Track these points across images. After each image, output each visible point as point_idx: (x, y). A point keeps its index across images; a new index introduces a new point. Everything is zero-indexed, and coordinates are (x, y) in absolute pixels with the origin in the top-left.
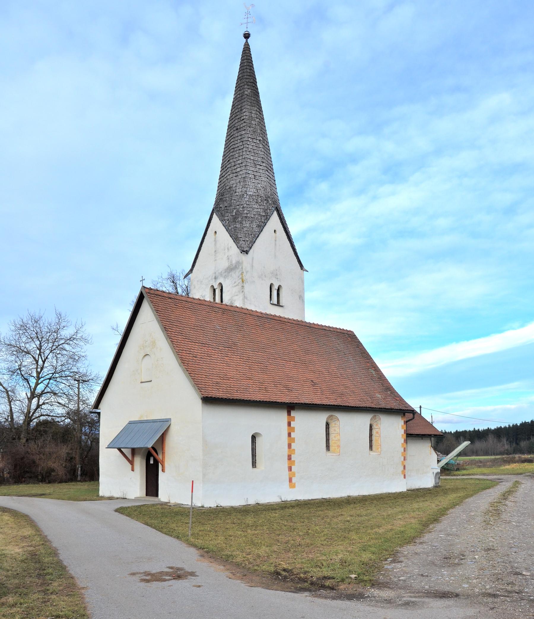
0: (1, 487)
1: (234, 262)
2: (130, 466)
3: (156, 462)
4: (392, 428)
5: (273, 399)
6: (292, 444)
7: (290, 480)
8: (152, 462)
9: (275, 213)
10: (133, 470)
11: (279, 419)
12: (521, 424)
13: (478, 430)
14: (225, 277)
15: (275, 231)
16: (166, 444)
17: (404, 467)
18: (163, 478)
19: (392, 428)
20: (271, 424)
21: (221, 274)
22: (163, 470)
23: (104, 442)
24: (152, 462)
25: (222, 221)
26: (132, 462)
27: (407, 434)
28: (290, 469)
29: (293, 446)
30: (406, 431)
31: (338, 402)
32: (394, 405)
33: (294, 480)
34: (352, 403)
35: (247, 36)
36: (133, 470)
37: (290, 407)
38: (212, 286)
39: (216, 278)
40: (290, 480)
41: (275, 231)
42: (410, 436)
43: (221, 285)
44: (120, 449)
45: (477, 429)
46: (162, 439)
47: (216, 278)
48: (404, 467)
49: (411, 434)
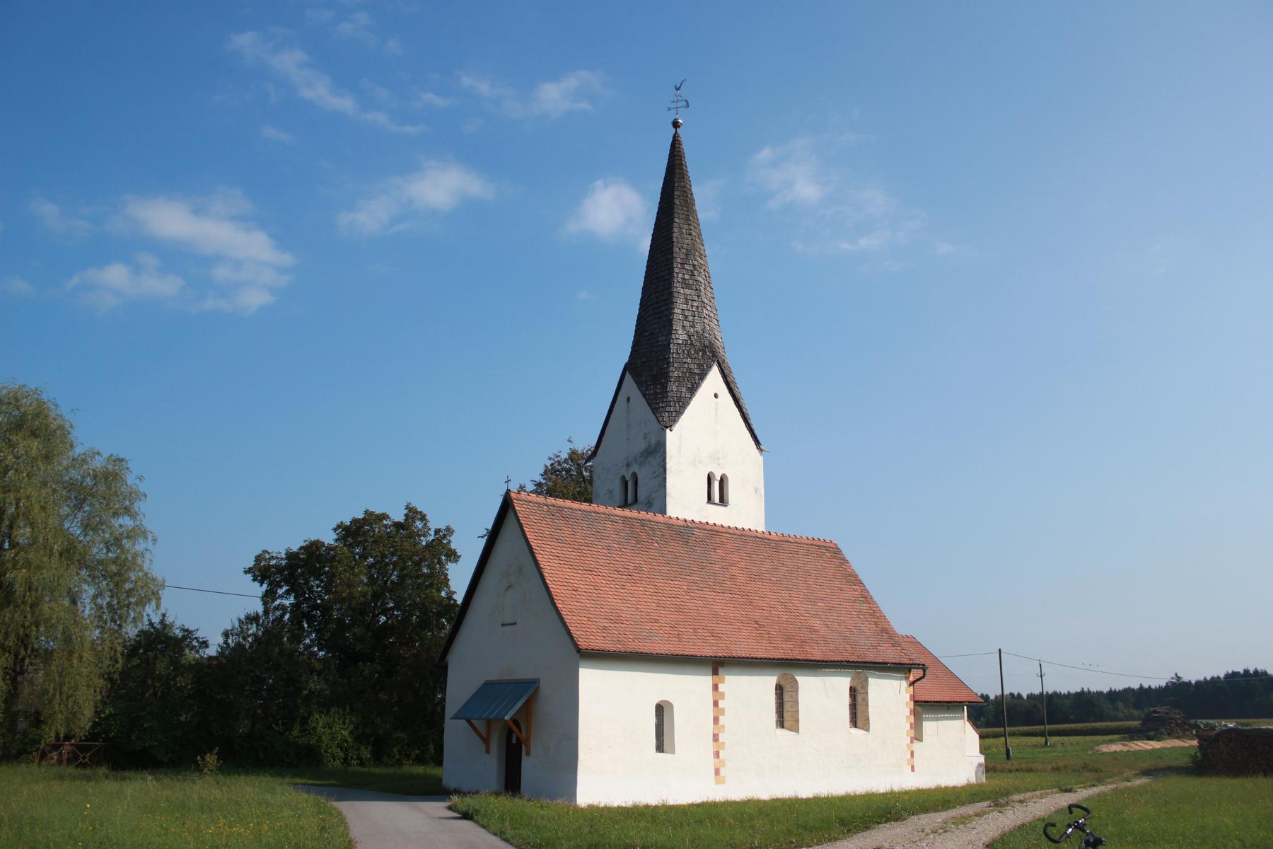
1: (653, 442)
2: (484, 746)
3: (519, 743)
4: (889, 696)
5: (689, 650)
6: (721, 718)
7: (717, 772)
8: (514, 741)
9: (715, 369)
10: (488, 751)
11: (700, 683)
12: (1227, 676)
13: (1141, 687)
15: (716, 396)
17: (912, 754)
18: (527, 764)
19: (889, 696)
20: (687, 691)
22: (528, 753)
23: (451, 710)
24: (514, 741)
26: (486, 741)
27: (916, 702)
28: (717, 755)
29: (722, 720)
30: (913, 697)
31: (796, 654)
34: (818, 655)
36: (488, 751)
37: (717, 665)
38: (623, 477)
39: (628, 465)
40: (717, 772)
41: (716, 396)
42: (924, 707)
43: (635, 476)
45: (1146, 686)
47: (628, 465)
48: (912, 754)
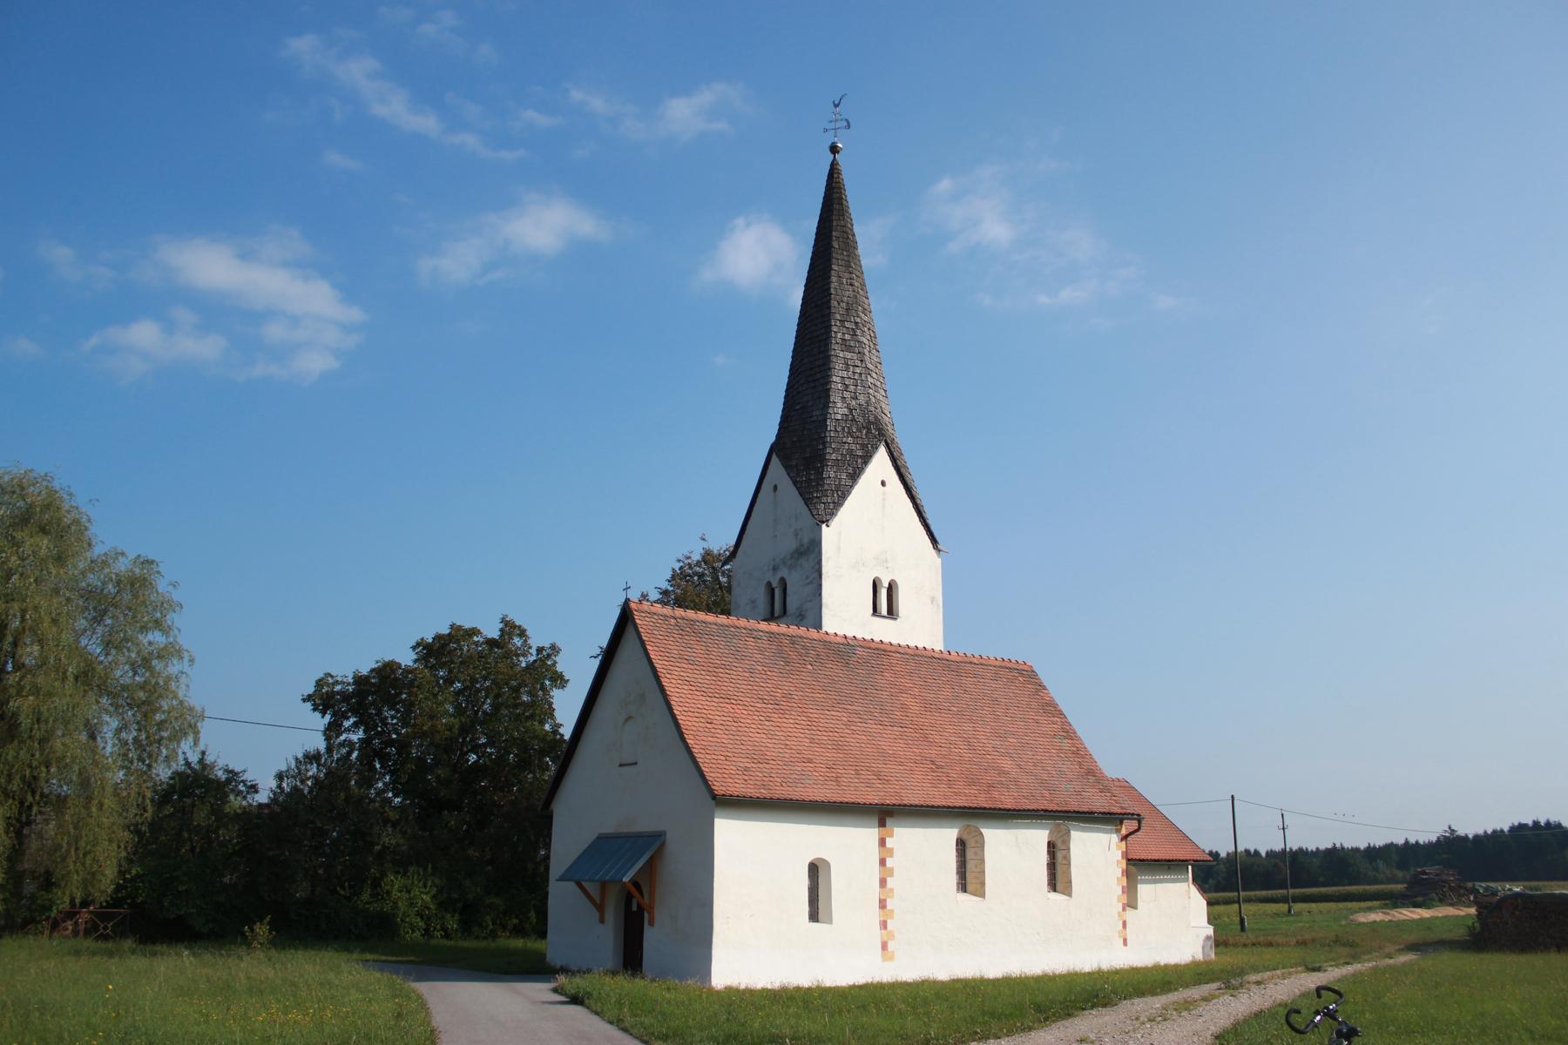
0: (4, 941)
1: (806, 540)
2: (597, 914)
3: (641, 909)
5: (849, 796)
8: (634, 908)
10: (602, 921)
12: (1512, 829)
14: (791, 568)
15: (883, 483)
16: (1098, 831)
17: (1124, 924)
18: (651, 936)
20: (848, 846)
21: (784, 561)
22: (651, 923)
23: (557, 867)
25: (786, 467)
26: (600, 908)
27: (1129, 861)
28: (884, 925)
29: (890, 882)
30: (1125, 855)
31: (982, 801)
32: (1099, 803)
33: (891, 946)
34: (1009, 803)
35: (834, 149)
36: (602, 921)
37: (883, 814)
39: (775, 569)
40: (884, 946)
41: (883, 483)
42: (1139, 867)
43: (783, 582)
44: (579, 884)
45: (1412, 841)
46: (651, 867)
47: (775, 569)
49: (1052, 867)
